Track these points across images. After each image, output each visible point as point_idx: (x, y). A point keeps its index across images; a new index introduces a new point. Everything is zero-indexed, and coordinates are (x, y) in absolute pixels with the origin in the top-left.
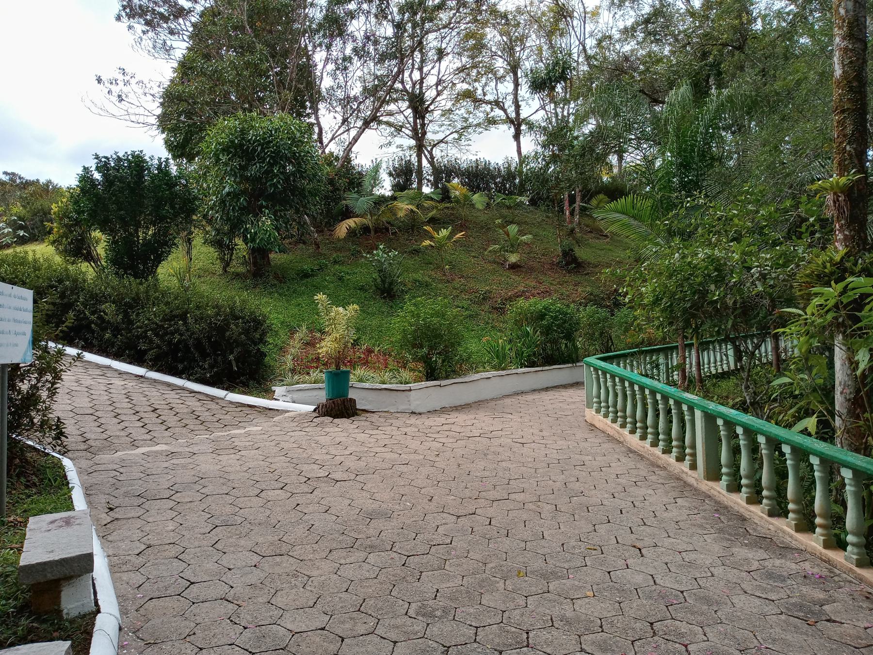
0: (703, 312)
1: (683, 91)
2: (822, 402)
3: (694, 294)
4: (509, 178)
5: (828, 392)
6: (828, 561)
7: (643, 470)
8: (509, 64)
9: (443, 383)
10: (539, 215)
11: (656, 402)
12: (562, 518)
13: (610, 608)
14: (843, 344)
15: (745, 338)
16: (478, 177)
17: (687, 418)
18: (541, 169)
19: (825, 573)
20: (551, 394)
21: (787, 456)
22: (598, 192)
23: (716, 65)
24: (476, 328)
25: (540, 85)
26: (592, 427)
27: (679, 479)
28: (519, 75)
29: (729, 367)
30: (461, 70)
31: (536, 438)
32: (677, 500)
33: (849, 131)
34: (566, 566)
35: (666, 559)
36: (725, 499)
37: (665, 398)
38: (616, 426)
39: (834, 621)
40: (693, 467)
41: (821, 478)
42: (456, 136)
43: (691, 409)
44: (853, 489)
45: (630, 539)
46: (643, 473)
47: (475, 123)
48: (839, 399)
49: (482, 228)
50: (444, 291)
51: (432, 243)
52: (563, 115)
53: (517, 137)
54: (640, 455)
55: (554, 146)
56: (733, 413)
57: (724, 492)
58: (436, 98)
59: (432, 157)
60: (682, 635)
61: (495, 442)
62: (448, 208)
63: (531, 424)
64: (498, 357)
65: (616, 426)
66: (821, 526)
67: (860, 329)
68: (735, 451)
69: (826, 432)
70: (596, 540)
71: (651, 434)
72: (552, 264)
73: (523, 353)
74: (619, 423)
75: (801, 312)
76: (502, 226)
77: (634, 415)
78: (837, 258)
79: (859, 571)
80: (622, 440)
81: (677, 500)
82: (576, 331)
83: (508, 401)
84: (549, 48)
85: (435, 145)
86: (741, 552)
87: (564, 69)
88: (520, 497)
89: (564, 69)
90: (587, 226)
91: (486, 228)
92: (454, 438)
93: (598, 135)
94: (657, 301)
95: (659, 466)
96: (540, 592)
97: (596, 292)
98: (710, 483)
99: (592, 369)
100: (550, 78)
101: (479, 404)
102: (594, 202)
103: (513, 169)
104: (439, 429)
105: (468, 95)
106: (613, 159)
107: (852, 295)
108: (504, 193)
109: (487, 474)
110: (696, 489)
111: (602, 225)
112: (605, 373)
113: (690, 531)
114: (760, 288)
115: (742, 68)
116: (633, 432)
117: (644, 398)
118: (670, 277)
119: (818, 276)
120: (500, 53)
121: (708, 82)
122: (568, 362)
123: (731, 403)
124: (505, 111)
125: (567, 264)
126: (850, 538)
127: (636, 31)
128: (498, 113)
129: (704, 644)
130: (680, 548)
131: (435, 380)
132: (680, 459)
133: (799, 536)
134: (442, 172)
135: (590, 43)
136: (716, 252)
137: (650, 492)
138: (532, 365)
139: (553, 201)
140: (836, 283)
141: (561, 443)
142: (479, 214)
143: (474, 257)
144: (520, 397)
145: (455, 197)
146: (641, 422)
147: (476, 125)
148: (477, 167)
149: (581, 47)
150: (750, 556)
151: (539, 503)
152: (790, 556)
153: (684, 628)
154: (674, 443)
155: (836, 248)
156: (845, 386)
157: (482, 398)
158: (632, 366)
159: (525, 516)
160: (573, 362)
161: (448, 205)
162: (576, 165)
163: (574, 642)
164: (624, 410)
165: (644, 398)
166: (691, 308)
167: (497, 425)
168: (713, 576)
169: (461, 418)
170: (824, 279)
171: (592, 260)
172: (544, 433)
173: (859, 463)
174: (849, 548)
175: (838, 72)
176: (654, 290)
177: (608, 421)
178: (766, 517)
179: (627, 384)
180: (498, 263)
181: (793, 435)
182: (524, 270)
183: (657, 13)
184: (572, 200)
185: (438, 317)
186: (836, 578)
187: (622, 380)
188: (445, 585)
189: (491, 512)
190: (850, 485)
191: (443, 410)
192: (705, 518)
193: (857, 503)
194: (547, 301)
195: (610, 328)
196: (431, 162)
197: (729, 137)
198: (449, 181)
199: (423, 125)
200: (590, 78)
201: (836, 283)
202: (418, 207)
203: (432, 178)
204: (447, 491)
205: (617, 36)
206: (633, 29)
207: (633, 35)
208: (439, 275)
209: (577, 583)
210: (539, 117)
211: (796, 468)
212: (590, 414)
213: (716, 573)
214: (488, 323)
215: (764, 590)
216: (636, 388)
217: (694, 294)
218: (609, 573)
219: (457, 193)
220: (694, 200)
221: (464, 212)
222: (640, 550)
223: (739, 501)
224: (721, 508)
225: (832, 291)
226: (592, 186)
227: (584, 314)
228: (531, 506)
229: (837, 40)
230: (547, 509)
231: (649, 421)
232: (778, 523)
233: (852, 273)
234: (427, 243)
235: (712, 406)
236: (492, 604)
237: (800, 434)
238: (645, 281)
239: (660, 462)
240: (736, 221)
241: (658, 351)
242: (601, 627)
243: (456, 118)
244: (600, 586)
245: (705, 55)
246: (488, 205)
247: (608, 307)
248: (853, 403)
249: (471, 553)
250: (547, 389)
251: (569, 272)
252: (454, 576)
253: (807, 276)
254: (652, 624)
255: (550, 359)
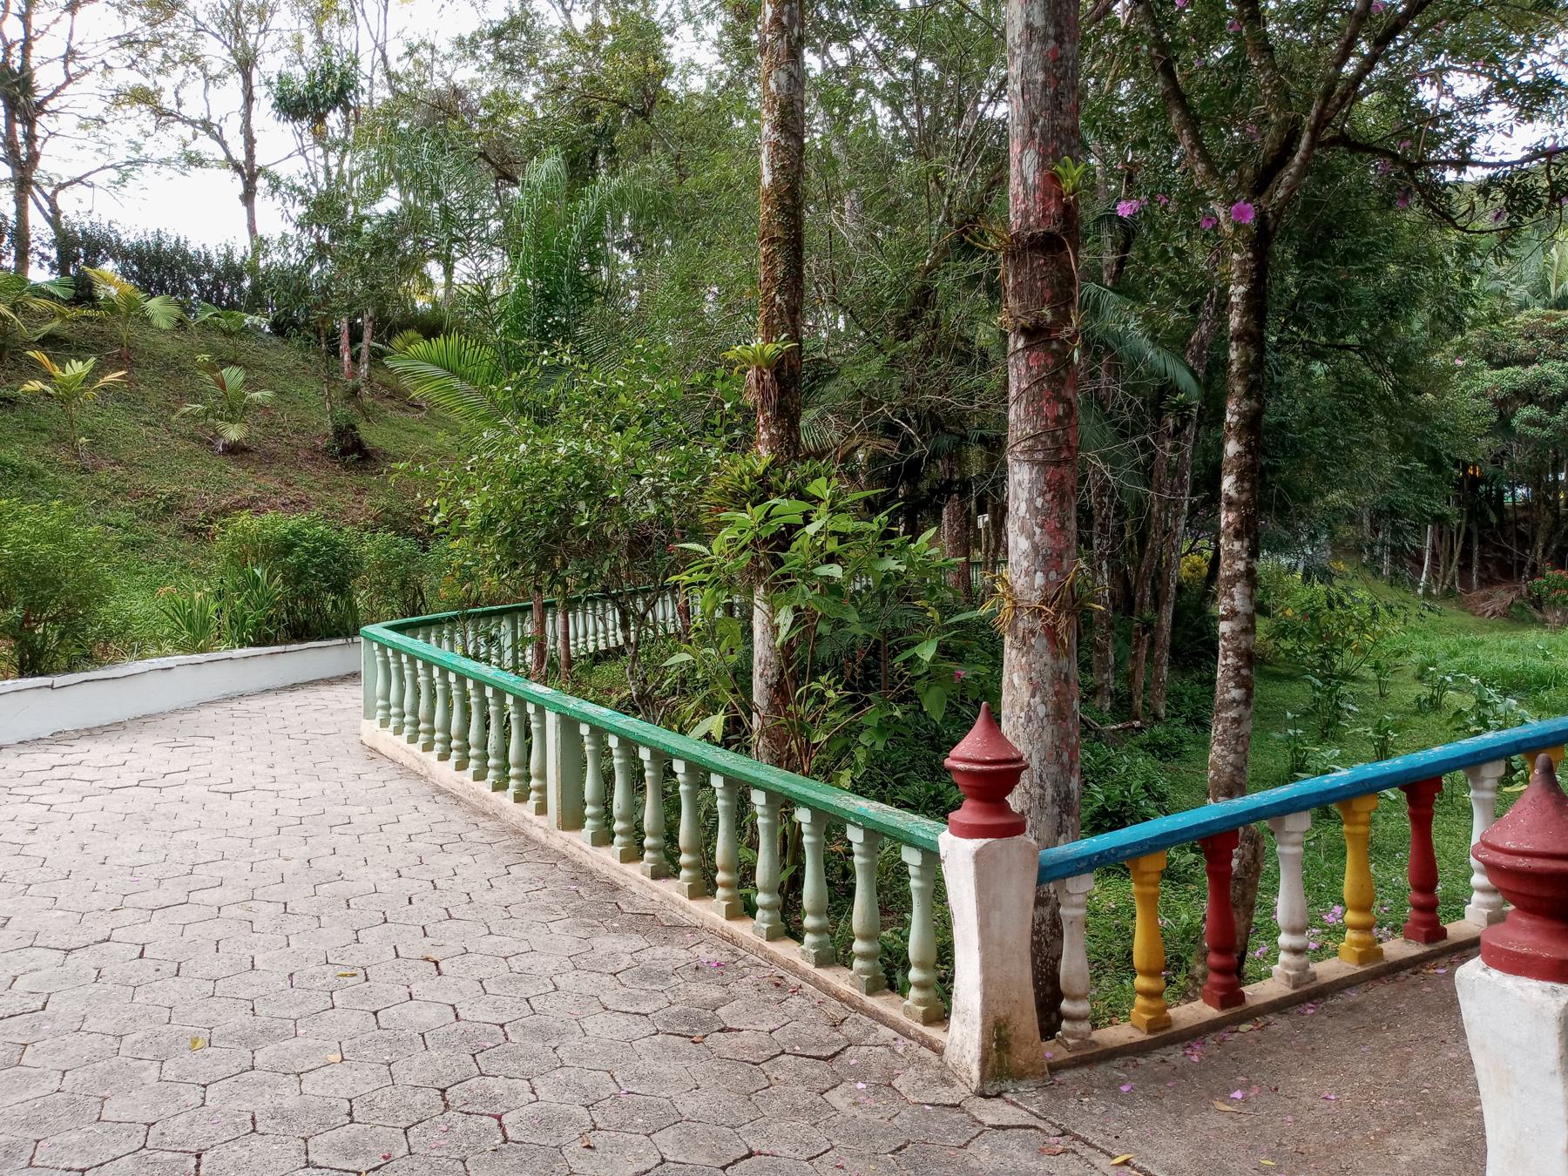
0: (576, 550)
1: (547, 167)
2: (734, 691)
3: (552, 514)
4: (228, 275)
5: (742, 675)
6: (731, 939)
7: (458, 820)
8: (233, 53)
9: (59, 680)
10: (286, 355)
11: (484, 702)
12: (292, 926)
13: (372, 1076)
14: (765, 601)
15: (634, 594)
16: (158, 267)
17: (534, 726)
18: (294, 268)
19: (726, 957)
20: (300, 696)
21: (680, 778)
22: (408, 327)
23: (605, 134)
24: (146, 568)
25: (301, 106)
26: (373, 753)
27: (516, 832)
28: (255, 81)
29: (607, 643)
30: (129, 41)
31: (260, 782)
32: (511, 869)
33: (779, 272)
34: (294, 1014)
35: (481, 973)
36: (588, 859)
37: (500, 694)
38: (416, 748)
39: (731, 1030)
40: (542, 809)
41: (726, 808)
42: (114, 175)
43: (540, 710)
44: (766, 821)
45: (422, 946)
46: (456, 828)
47: (156, 157)
48: (758, 685)
49: (168, 367)
50: (75, 489)
51: (50, 390)
52: (340, 174)
53: (248, 197)
54: (454, 797)
55: (319, 226)
56: (604, 714)
57: (588, 847)
58: (63, 87)
59: (56, 211)
60: (494, 1100)
61: (171, 794)
62: (90, 319)
63: (251, 755)
64: (190, 627)
65: (416, 748)
66: (724, 885)
67: (785, 576)
68: (607, 778)
69: (735, 736)
70: (357, 957)
71: (475, 757)
72: (315, 449)
73: (245, 618)
74: (421, 743)
75: (704, 549)
76: (211, 368)
77: (446, 728)
78: (760, 469)
79: (770, 946)
80: (424, 772)
81: (511, 869)
82: (354, 577)
83: (208, 713)
84: (316, 42)
85: (62, 186)
86: (606, 943)
87: (342, 90)
88: (214, 896)
89: (342, 90)
90: (384, 386)
91: (175, 368)
92: (75, 792)
93: (411, 221)
94: (488, 524)
95: (485, 814)
96: (235, 1071)
97: (397, 507)
98: (566, 834)
99: (375, 646)
100: (315, 98)
101: (143, 721)
102: (398, 342)
103: (237, 260)
104: (41, 777)
105: (142, 96)
106: (434, 269)
107: (776, 525)
108: (218, 304)
109: (144, 858)
110: (544, 848)
111: (406, 382)
112: (397, 653)
113: (527, 919)
114: (653, 511)
115: (647, 148)
116: (444, 757)
117: (465, 697)
118: (515, 482)
119: (733, 494)
120: (213, 27)
121: (593, 159)
122: (338, 636)
123: (615, 698)
124: (224, 144)
125: (344, 452)
126: (761, 899)
127: (478, 47)
128: (205, 145)
129: (529, 1108)
130: (507, 950)
131: (41, 675)
132: (521, 798)
133: (695, 905)
134: (76, 243)
135: (395, 50)
136: (588, 447)
137: (467, 859)
138: (263, 640)
139: (317, 332)
140: (753, 506)
141: (311, 787)
142: (160, 338)
143: (147, 424)
144: (235, 705)
145: (108, 298)
146: (517, 765)
147: (161, 162)
148: (159, 245)
149: (378, 55)
150: (620, 947)
151: (251, 904)
152: (678, 939)
153: (498, 1086)
154: (513, 771)
155: (758, 453)
156: (767, 664)
157: (147, 712)
158: (452, 640)
159: (218, 931)
160: (347, 635)
161: (90, 313)
162: (362, 268)
163: (294, 1153)
164: (464, 735)
165: (465, 697)
166: (547, 538)
167: (180, 759)
168: (556, 989)
169: (97, 752)
170: (738, 499)
171: (391, 448)
172: (277, 771)
173: (773, 780)
174: (759, 913)
175: (767, 179)
176: (485, 506)
177: (402, 740)
178: (648, 880)
179: (436, 672)
180: (201, 440)
181: (691, 745)
182: (256, 457)
183: (516, 25)
184: (356, 336)
185: (50, 541)
186: (740, 964)
187: (428, 666)
188: (16, 1099)
189: (143, 933)
190: (916, 877)
191: (59, 737)
192: (554, 894)
193: (816, 862)
194: (296, 520)
195: (420, 572)
196: (54, 218)
197: (626, 257)
198: (93, 265)
199: (31, 138)
200: (390, 112)
201: (753, 506)
202: (14, 308)
203: (53, 254)
204: (49, 903)
205: (445, 48)
206: (474, 43)
207: (473, 53)
208: (64, 456)
209: (311, 1042)
210: (292, 170)
211: (693, 795)
212: (373, 732)
213: (561, 985)
214: (173, 559)
215: (636, 1000)
216: (489, 692)
217: (552, 514)
218: (375, 1013)
219: (113, 291)
220: (554, 355)
221: (125, 331)
222: (436, 963)
223: (608, 859)
224: (582, 874)
225: (750, 517)
226: (394, 313)
227: (371, 548)
228: (236, 911)
229: (766, 128)
230: (266, 913)
231: (473, 736)
232: (668, 888)
233: (778, 493)
234: (36, 385)
235: (574, 704)
236: (125, 1116)
237: (697, 741)
238: (470, 489)
239: (488, 807)
240: (622, 398)
241: (500, 614)
242: (350, 1114)
243: (114, 139)
244: (357, 1041)
245: (589, 115)
246: (181, 324)
247: (418, 535)
248: (776, 691)
249: (91, 1020)
250: (293, 687)
251: (347, 467)
252: (42, 1075)
253: (719, 494)
254: (444, 1091)
255: (301, 631)
